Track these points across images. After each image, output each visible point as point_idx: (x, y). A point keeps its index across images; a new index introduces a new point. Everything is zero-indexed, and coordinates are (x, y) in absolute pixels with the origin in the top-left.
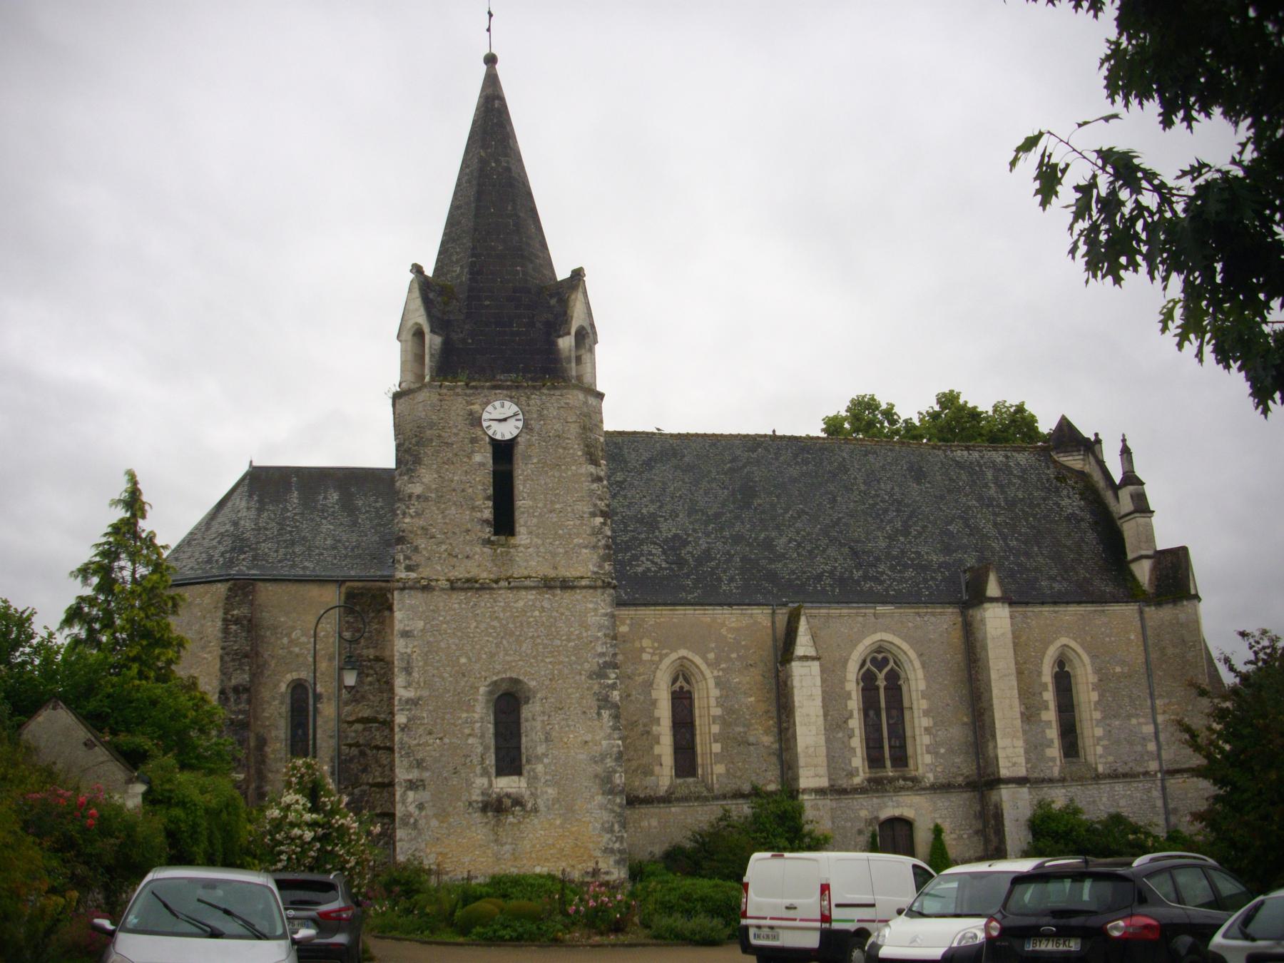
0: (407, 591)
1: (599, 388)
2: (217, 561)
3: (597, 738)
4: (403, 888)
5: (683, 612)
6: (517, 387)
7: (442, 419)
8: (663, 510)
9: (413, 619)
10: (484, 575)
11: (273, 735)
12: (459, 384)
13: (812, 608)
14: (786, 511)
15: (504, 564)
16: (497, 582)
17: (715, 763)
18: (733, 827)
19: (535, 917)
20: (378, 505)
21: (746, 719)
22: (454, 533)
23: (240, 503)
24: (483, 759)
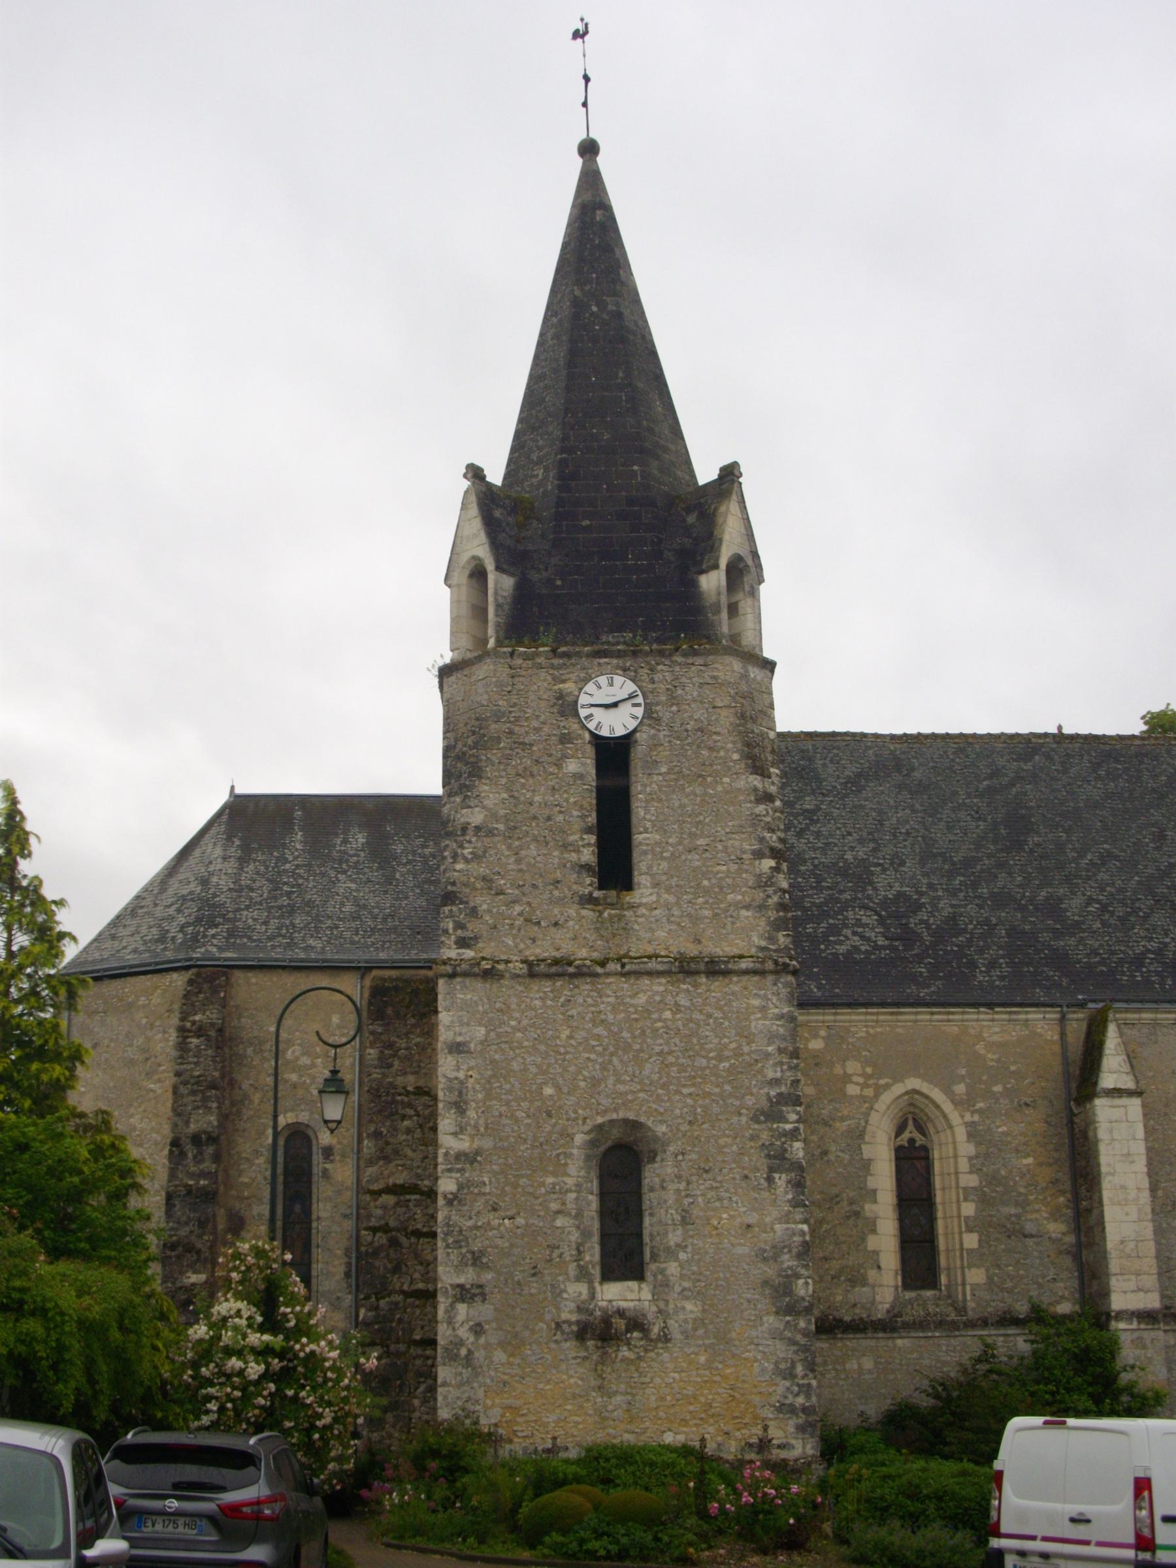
0: (459, 979)
1: (768, 653)
2: (173, 938)
3: (768, 1219)
4: (445, 1464)
5: (912, 1017)
6: (635, 654)
7: (515, 705)
8: (880, 854)
9: (468, 1024)
10: (583, 953)
11: (255, 1213)
12: (541, 649)
13: (1127, 1010)
14: (1082, 853)
15: (614, 935)
16: (603, 963)
17: (969, 1267)
18: (999, 1373)
19: (651, 1520)
20: (427, 851)
21: (1020, 1194)
22: (534, 886)
23: (214, 850)
24: (579, 1252)
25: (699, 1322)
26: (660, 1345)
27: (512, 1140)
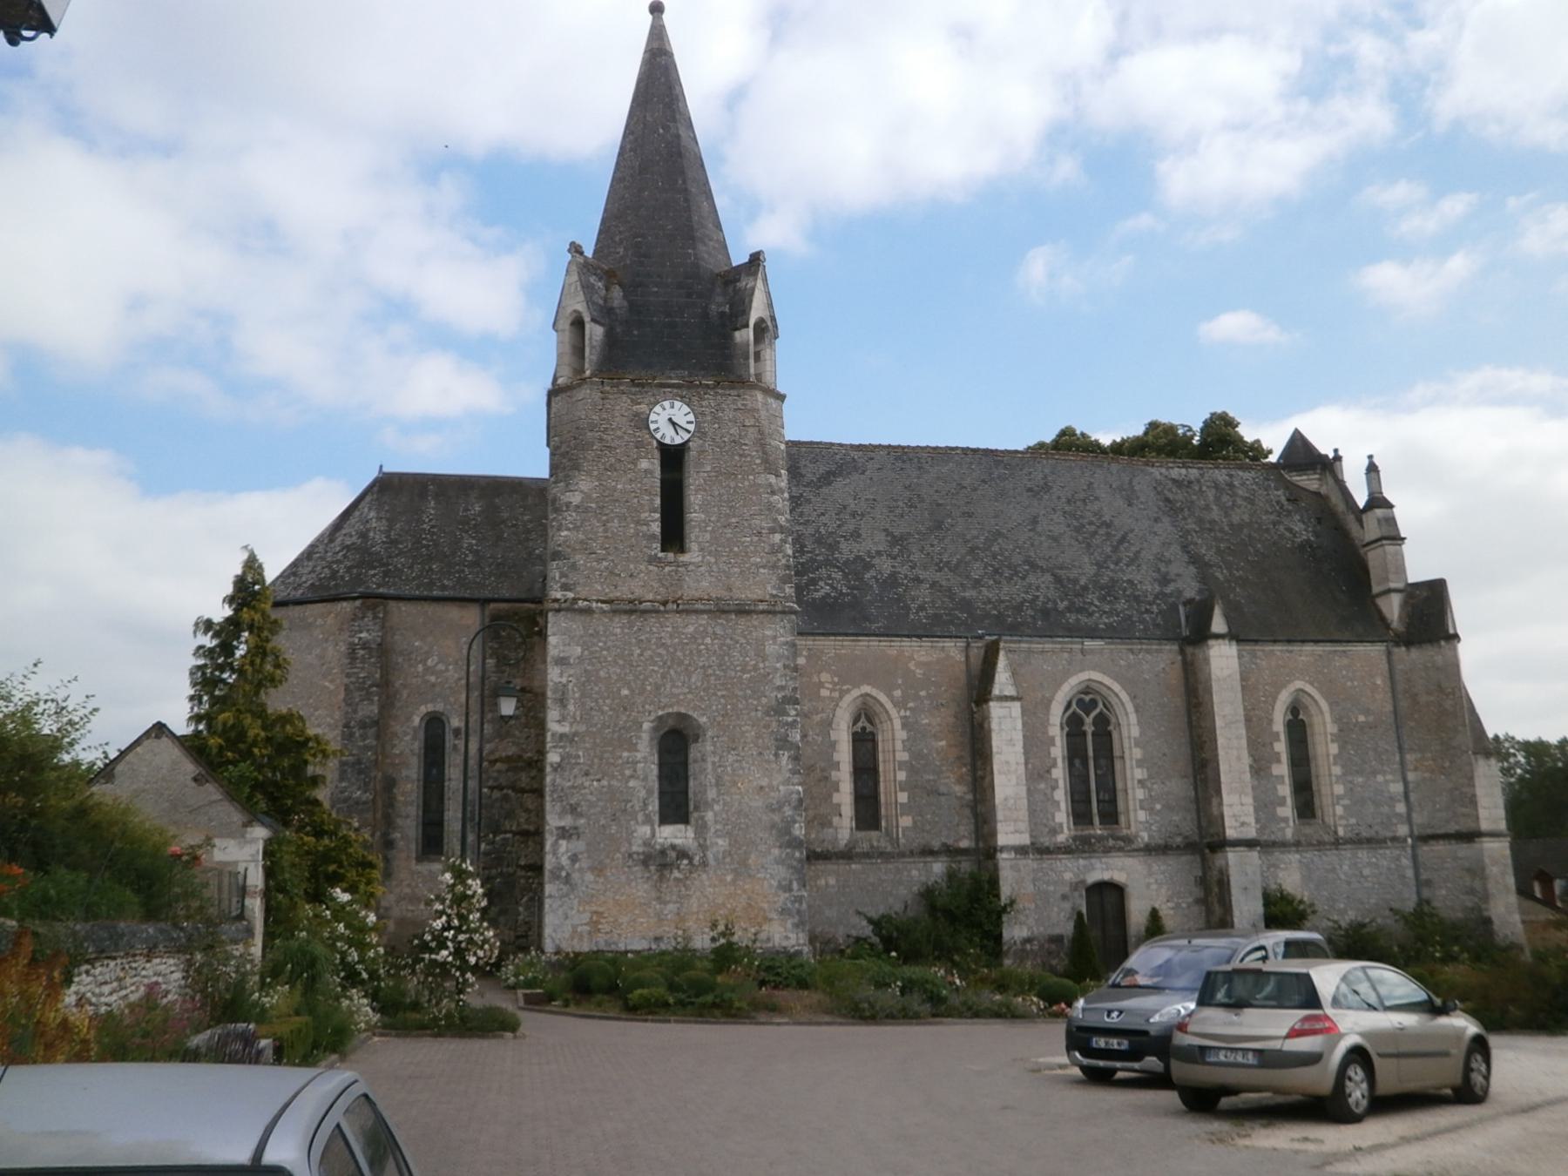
0: (562, 613)
1: (781, 389)
5: (866, 643)
7: (604, 419)
9: (569, 645)
16: (665, 603)
25: (727, 853)
27: (599, 726)
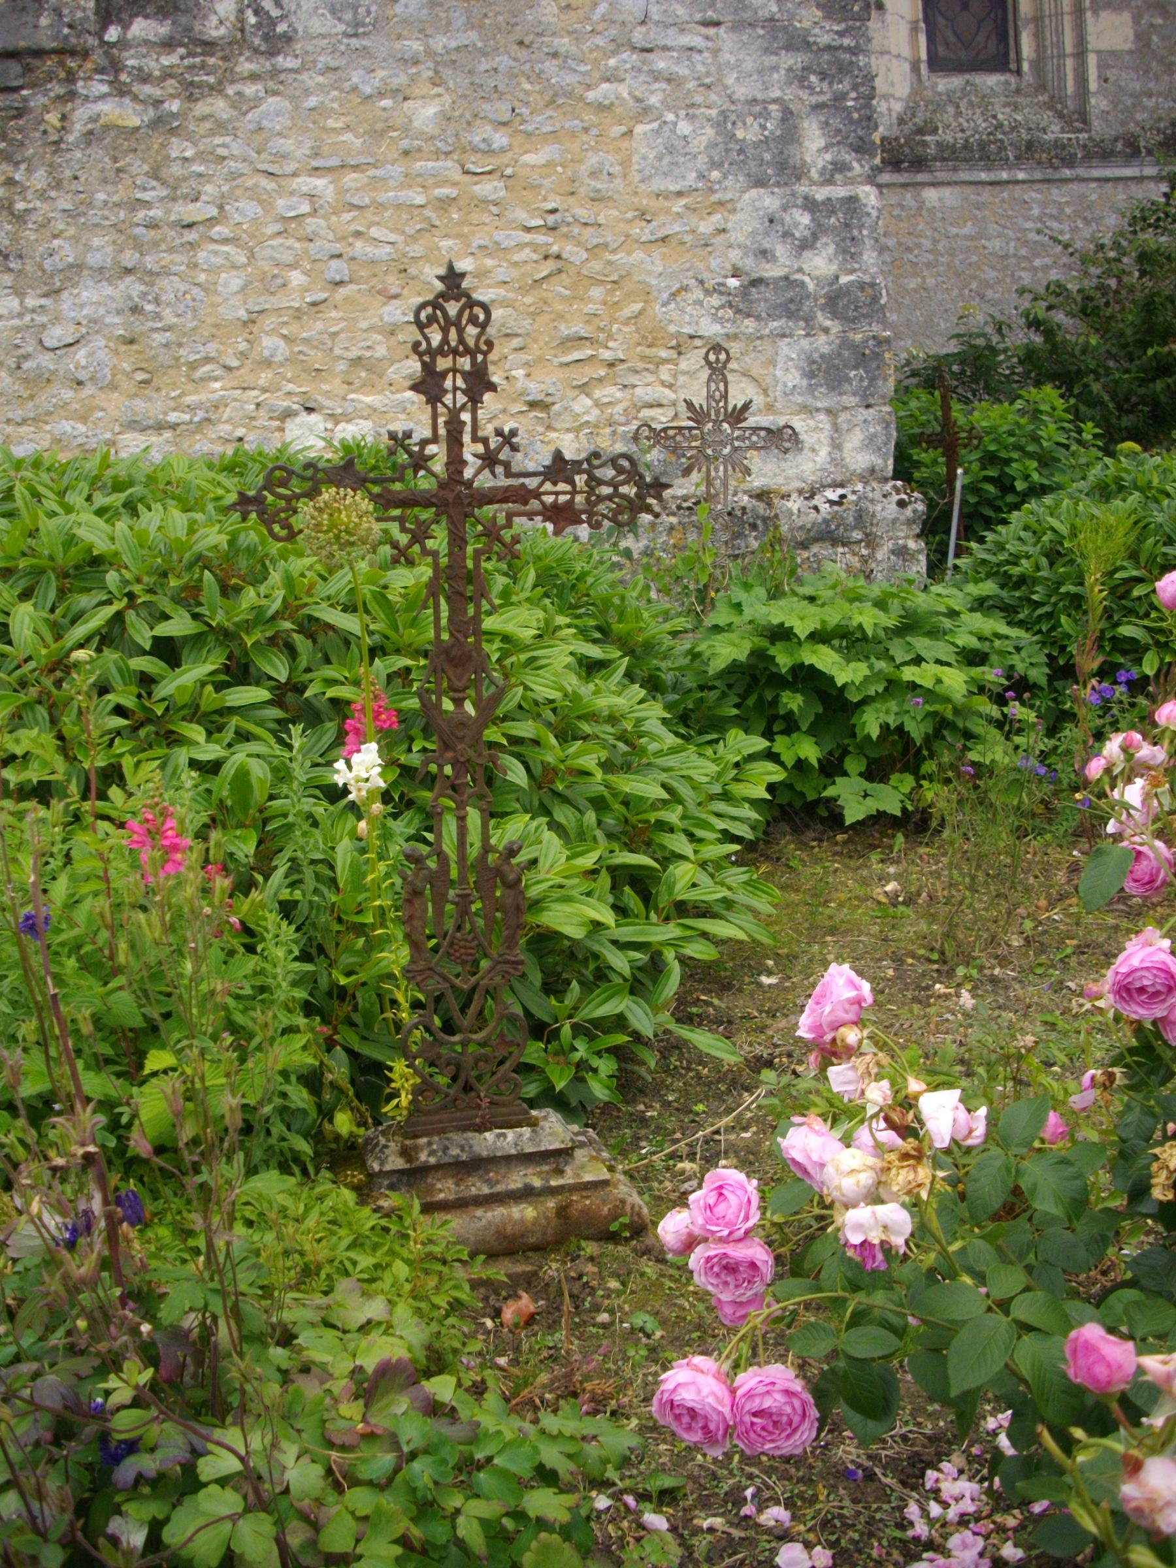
26: (245, 66)
